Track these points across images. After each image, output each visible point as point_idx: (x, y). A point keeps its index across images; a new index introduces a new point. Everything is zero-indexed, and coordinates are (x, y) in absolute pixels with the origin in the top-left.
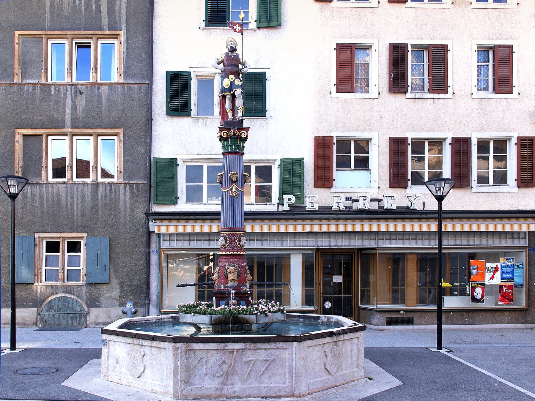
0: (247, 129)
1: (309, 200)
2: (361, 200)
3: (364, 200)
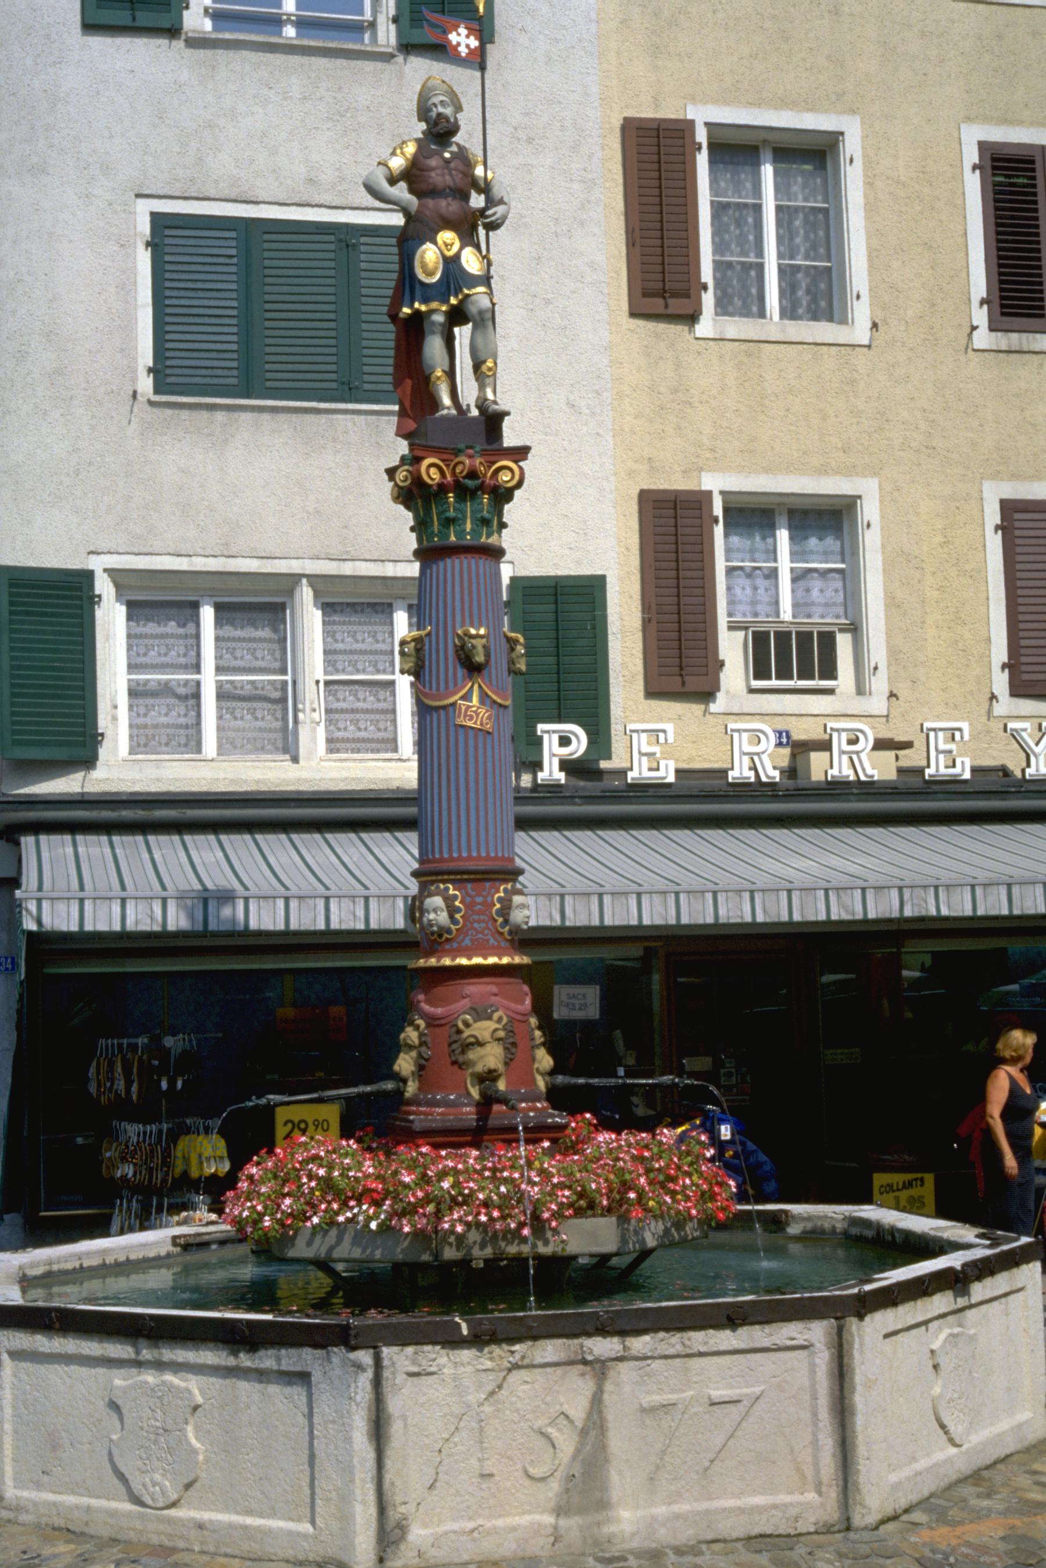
0: (521, 453)
1: (642, 742)
2: (839, 742)
3: (851, 742)
